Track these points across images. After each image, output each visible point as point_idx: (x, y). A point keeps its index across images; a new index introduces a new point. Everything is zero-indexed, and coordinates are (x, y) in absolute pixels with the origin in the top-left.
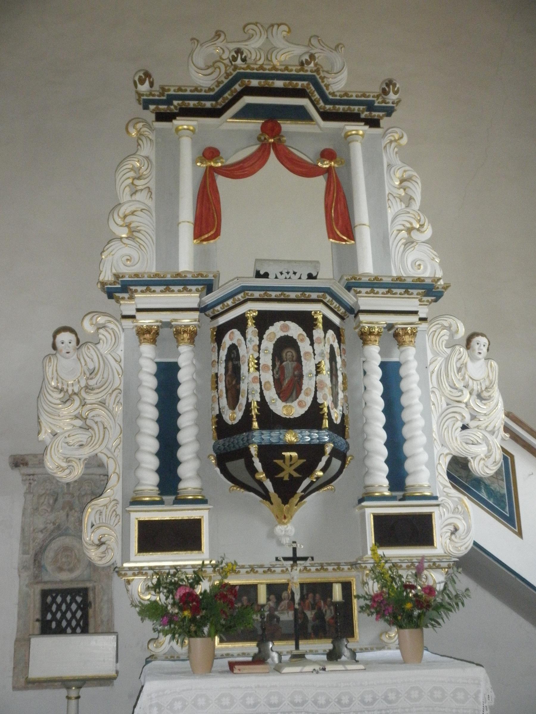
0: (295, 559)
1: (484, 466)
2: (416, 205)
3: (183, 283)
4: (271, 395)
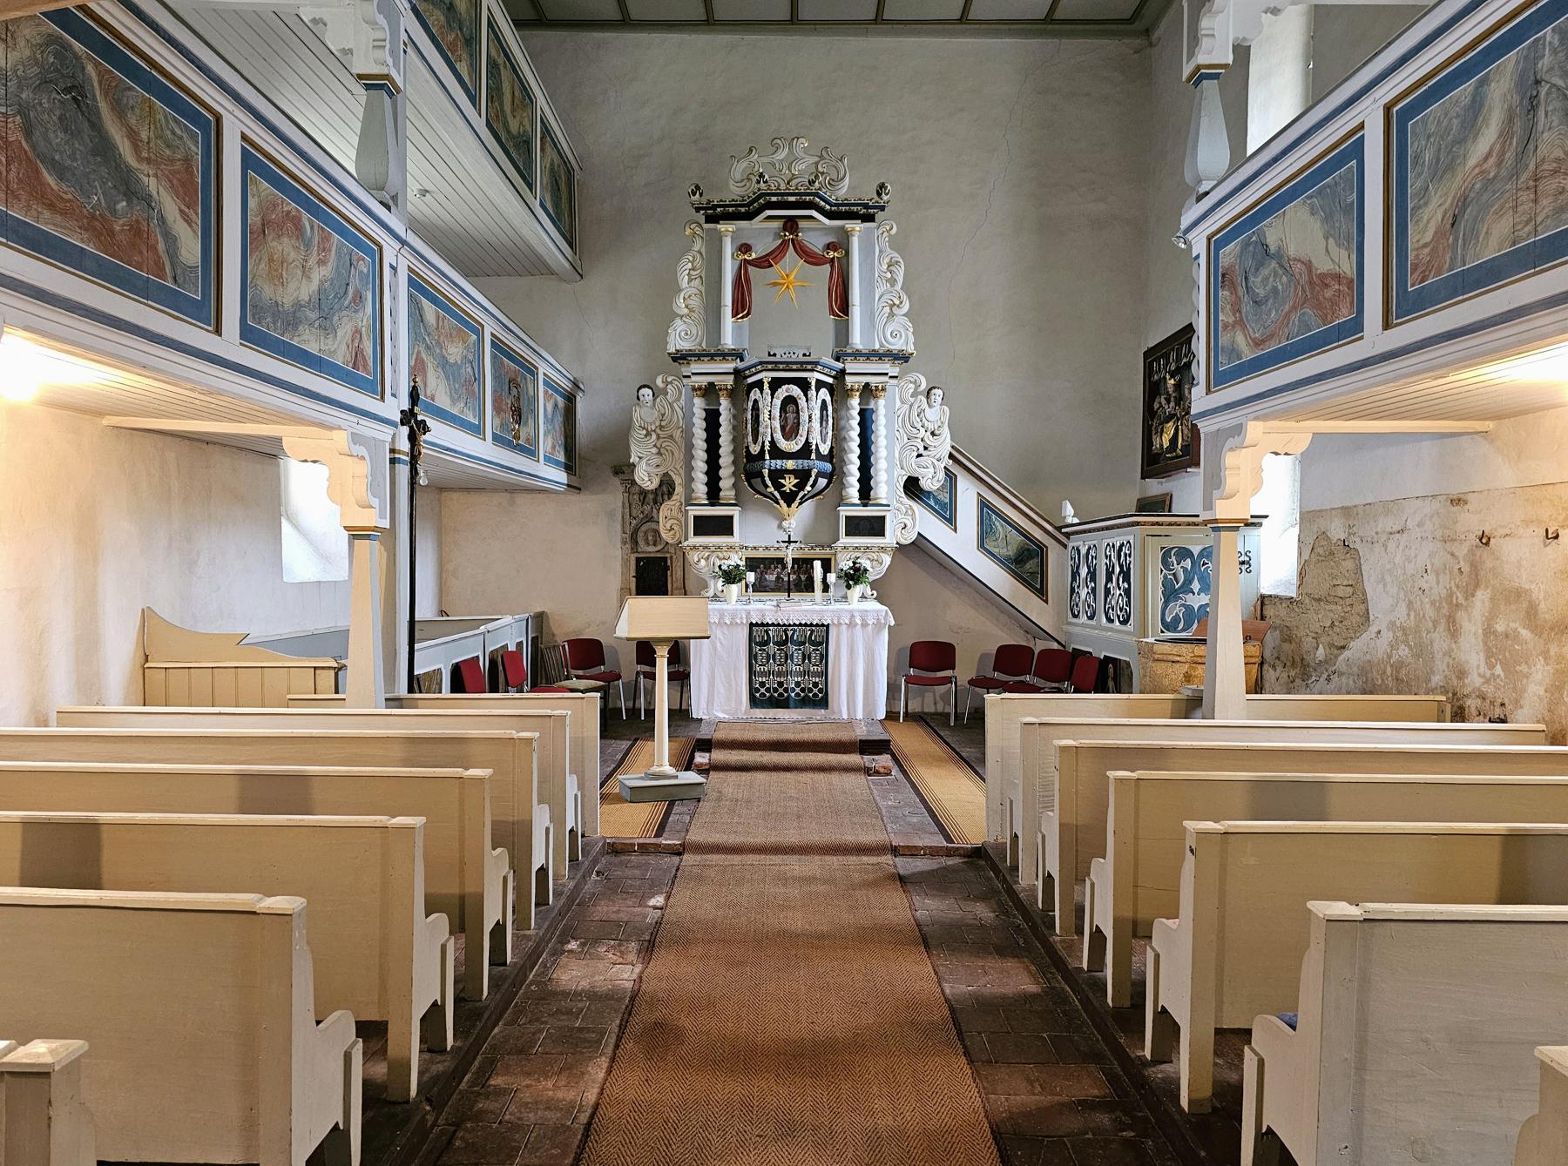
0: (789, 542)
1: (931, 481)
3: (724, 355)
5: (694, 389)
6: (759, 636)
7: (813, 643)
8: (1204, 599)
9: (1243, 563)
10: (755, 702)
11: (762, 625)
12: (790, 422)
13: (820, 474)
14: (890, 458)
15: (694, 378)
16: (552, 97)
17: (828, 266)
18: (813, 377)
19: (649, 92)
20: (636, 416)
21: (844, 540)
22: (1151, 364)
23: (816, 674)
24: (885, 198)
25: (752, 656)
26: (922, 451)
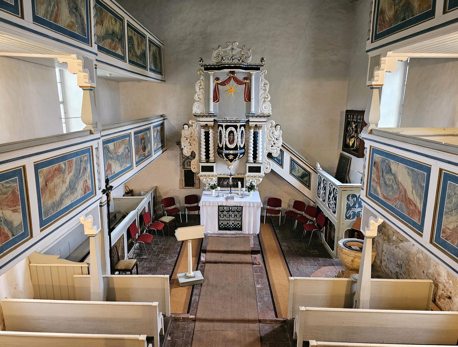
2: (267, 92)
4: (228, 143)
5: (201, 126)
6: (221, 210)
7: (237, 211)
8: (359, 210)
10: (220, 229)
11: (222, 206)
12: (231, 139)
13: (241, 154)
14: (263, 148)
16: (151, 31)
21: (248, 174)
22: (348, 115)
23: (238, 221)
24: (263, 63)
25: (219, 215)
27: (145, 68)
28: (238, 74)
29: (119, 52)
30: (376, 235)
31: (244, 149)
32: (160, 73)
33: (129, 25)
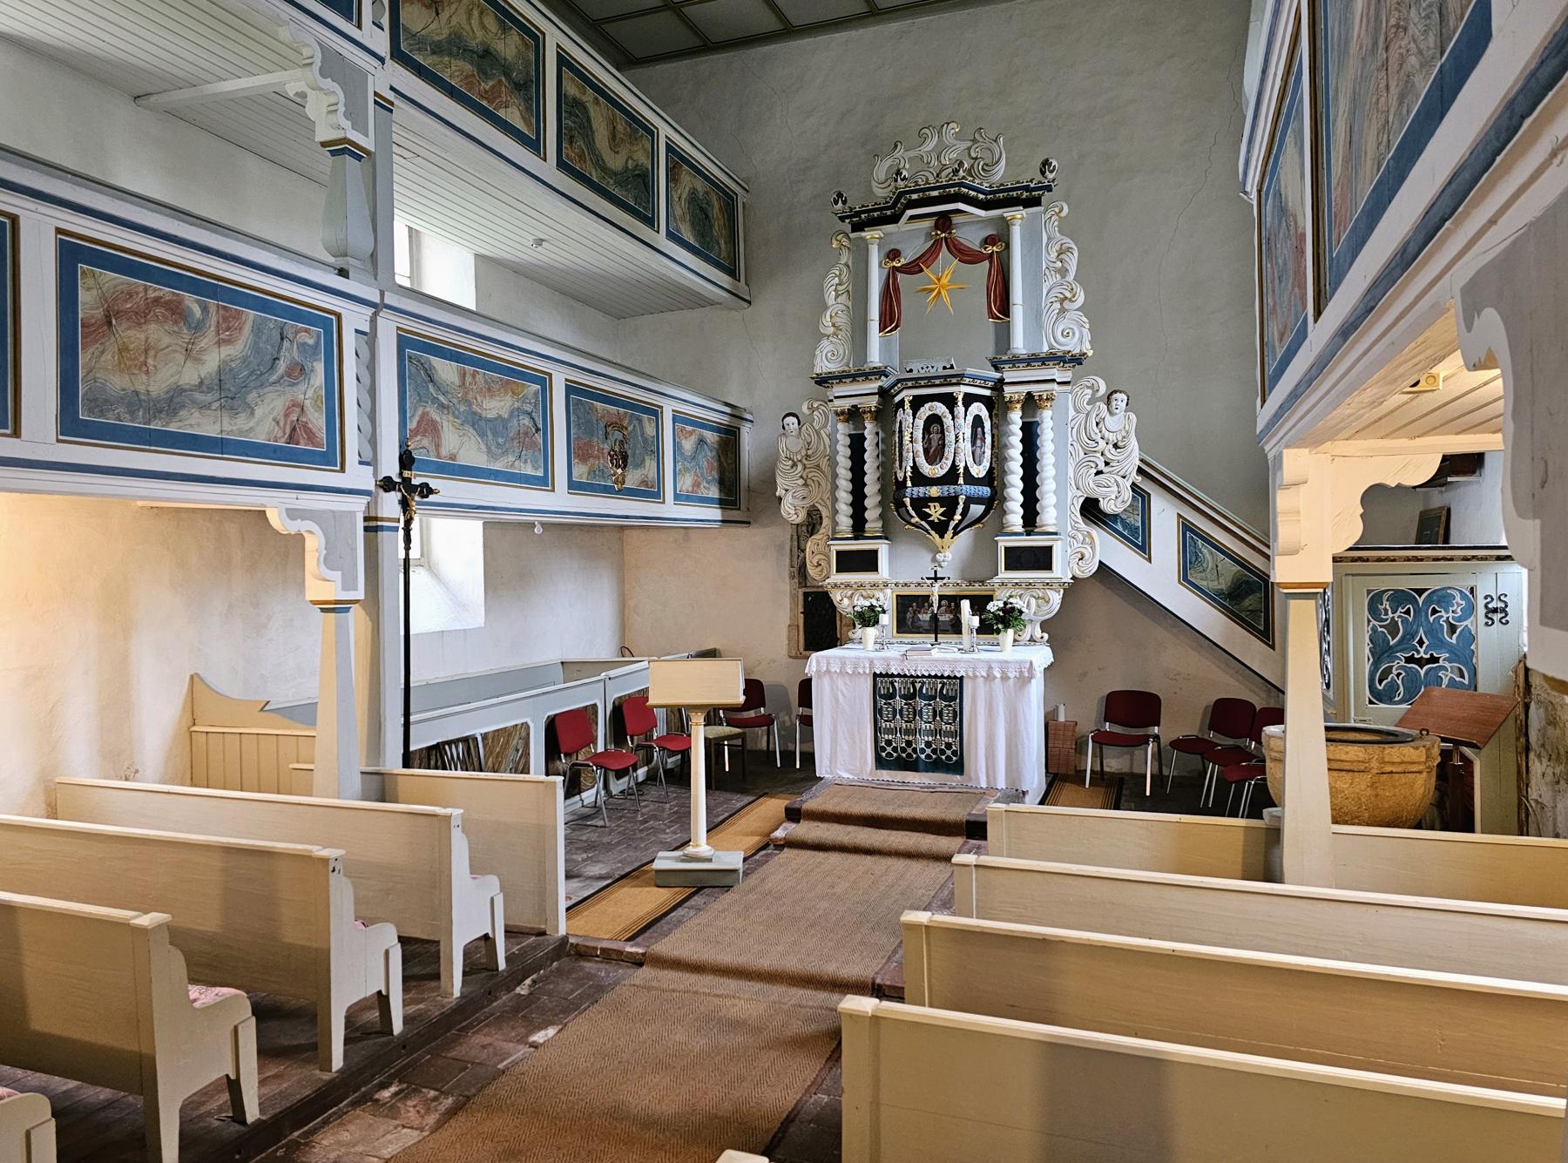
0: (936, 579)
5: (837, 414)
9: (1495, 610)
10: (881, 763)
11: (887, 675)
12: (934, 444)
14: (1060, 478)
15: (836, 402)
16: (680, 119)
17: (986, 263)
18: (960, 391)
19: (812, 105)
20: (782, 446)
21: (1004, 575)
24: (1051, 176)
25: (877, 711)
26: (1102, 466)
27: (650, 222)
28: (965, 228)
29: (513, 116)
30: (1330, 580)
31: (990, 485)
32: (732, 272)
33: (563, 61)
